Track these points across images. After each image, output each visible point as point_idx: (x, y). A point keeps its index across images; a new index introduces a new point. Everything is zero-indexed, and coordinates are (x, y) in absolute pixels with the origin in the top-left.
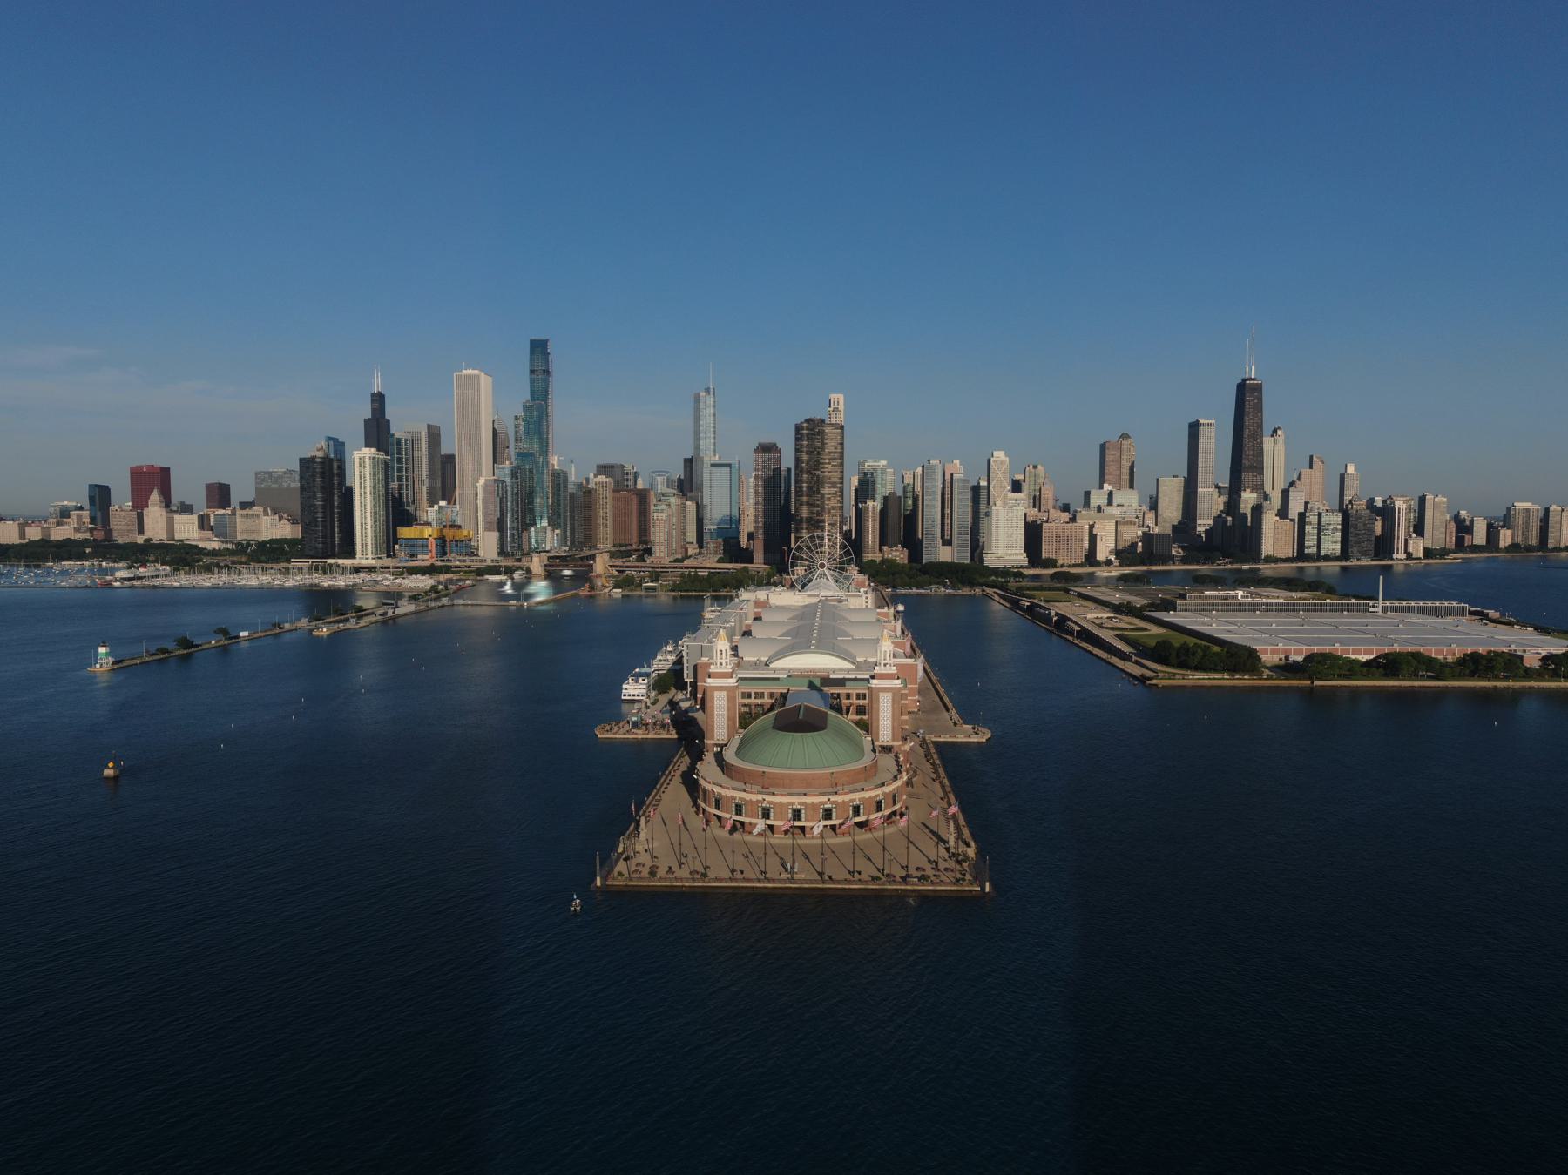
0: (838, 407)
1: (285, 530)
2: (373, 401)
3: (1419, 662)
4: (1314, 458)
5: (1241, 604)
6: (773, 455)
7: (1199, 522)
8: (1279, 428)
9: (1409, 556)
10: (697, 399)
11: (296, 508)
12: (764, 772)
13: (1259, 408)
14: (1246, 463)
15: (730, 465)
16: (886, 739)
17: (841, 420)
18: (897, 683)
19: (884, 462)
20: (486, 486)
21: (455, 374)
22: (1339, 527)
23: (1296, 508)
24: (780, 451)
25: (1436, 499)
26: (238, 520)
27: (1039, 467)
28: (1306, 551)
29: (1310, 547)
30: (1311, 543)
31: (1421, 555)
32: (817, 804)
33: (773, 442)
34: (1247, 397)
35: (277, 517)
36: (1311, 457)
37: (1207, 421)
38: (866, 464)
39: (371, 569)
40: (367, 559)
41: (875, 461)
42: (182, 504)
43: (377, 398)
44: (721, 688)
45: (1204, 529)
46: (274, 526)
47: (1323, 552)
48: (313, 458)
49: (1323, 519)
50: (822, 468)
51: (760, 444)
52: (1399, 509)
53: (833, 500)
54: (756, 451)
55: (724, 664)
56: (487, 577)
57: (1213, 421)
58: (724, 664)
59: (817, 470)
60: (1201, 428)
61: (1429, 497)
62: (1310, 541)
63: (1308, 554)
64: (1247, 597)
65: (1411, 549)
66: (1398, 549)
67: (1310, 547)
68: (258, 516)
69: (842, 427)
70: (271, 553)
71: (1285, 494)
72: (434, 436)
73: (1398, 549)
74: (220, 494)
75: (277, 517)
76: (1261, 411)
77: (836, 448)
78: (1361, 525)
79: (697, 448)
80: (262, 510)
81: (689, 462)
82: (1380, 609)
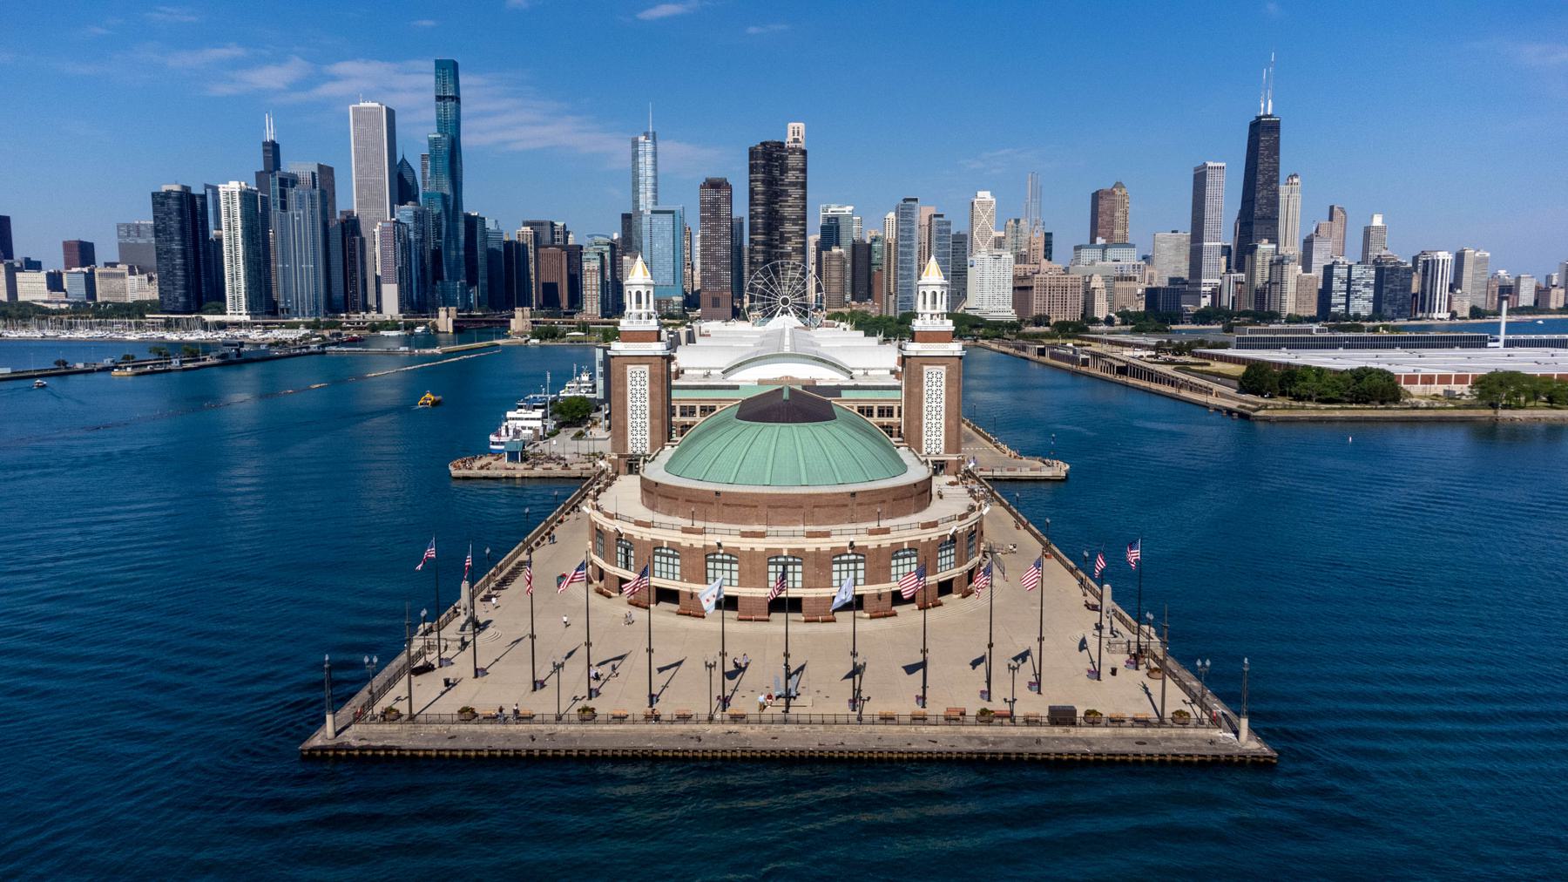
0: (794, 132)
1: (151, 293)
2: (265, 151)
3: (617, 702)
4: (1335, 209)
5: (1315, 339)
6: (725, 193)
7: (1204, 281)
8: (1296, 176)
9: (1454, 315)
10: (635, 143)
11: (152, 260)
12: (717, 493)
13: (1275, 149)
14: (1257, 212)
15: (672, 212)
16: (933, 449)
17: (802, 145)
18: (955, 348)
19: (851, 208)
20: (383, 230)
21: (351, 108)
22: (1372, 282)
23: (1319, 260)
24: (730, 188)
25: (1477, 255)
26: (97, 279)
27: (1022, 222)
28: (1333, 309)
29: (1336, 305)
30: (1338, 301)
31: (1466, 314)
32: (826, 554)
33: (723, 177)
34: (1263, 135)
35: (145, 277)
36: (1332, 208)
37: (1216, 164)
38: (830, 210)
39: (238, 325)
40: (241, 314)
41: (840, 207)
42: (27, 260)
43: (270, 148)
44: (639, 359)
45: (1210, 289)
46: (141, 290)
47: (1351, 312)
48: (168, 193)
49: (1353, 272)
50: (781, 201)
51: (707, 180)
52: (1444, 260)
53: (794, 240)
54: (701, 187)
55: (644, 316)
56: (382, 333)
57: (1223, 164)
58: (644, 316)
59: (776, 203)
60: (1209, 172)
61: (1469, 252)
62: (1337, 299)
63: (1336, 314)
64: (1324, 331)
65: (1455, 307)
66: (1440, 305)
67: (1336, 305)
68: (122, 276)
69: (804, 153)
70: (135, 311)
71: (1308, 244)
72: (325, 176)
73: (1440, 305)
74: (83, 253)
75: (145, 277)
76: (1277, 153)
77: (797, 178)
78: (1398, 280)
79: (636, 201)
80: (127, 267)
81: (627, 218)
82: (1501, 344)
